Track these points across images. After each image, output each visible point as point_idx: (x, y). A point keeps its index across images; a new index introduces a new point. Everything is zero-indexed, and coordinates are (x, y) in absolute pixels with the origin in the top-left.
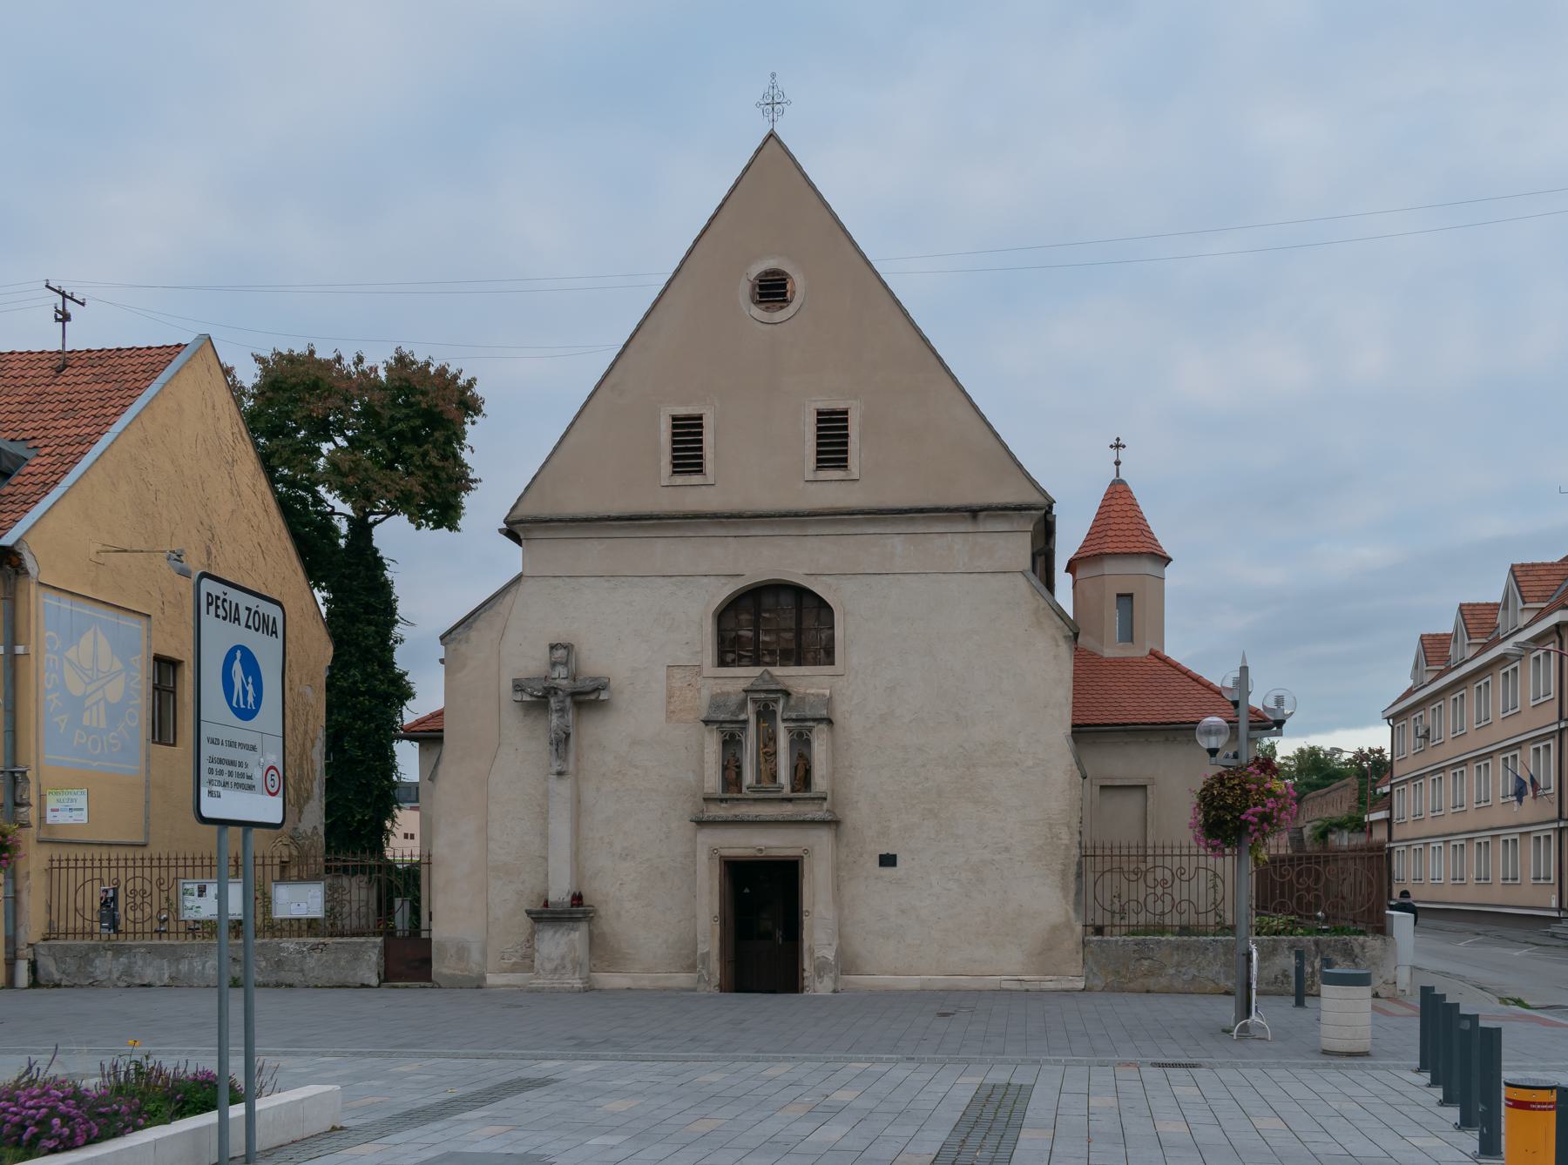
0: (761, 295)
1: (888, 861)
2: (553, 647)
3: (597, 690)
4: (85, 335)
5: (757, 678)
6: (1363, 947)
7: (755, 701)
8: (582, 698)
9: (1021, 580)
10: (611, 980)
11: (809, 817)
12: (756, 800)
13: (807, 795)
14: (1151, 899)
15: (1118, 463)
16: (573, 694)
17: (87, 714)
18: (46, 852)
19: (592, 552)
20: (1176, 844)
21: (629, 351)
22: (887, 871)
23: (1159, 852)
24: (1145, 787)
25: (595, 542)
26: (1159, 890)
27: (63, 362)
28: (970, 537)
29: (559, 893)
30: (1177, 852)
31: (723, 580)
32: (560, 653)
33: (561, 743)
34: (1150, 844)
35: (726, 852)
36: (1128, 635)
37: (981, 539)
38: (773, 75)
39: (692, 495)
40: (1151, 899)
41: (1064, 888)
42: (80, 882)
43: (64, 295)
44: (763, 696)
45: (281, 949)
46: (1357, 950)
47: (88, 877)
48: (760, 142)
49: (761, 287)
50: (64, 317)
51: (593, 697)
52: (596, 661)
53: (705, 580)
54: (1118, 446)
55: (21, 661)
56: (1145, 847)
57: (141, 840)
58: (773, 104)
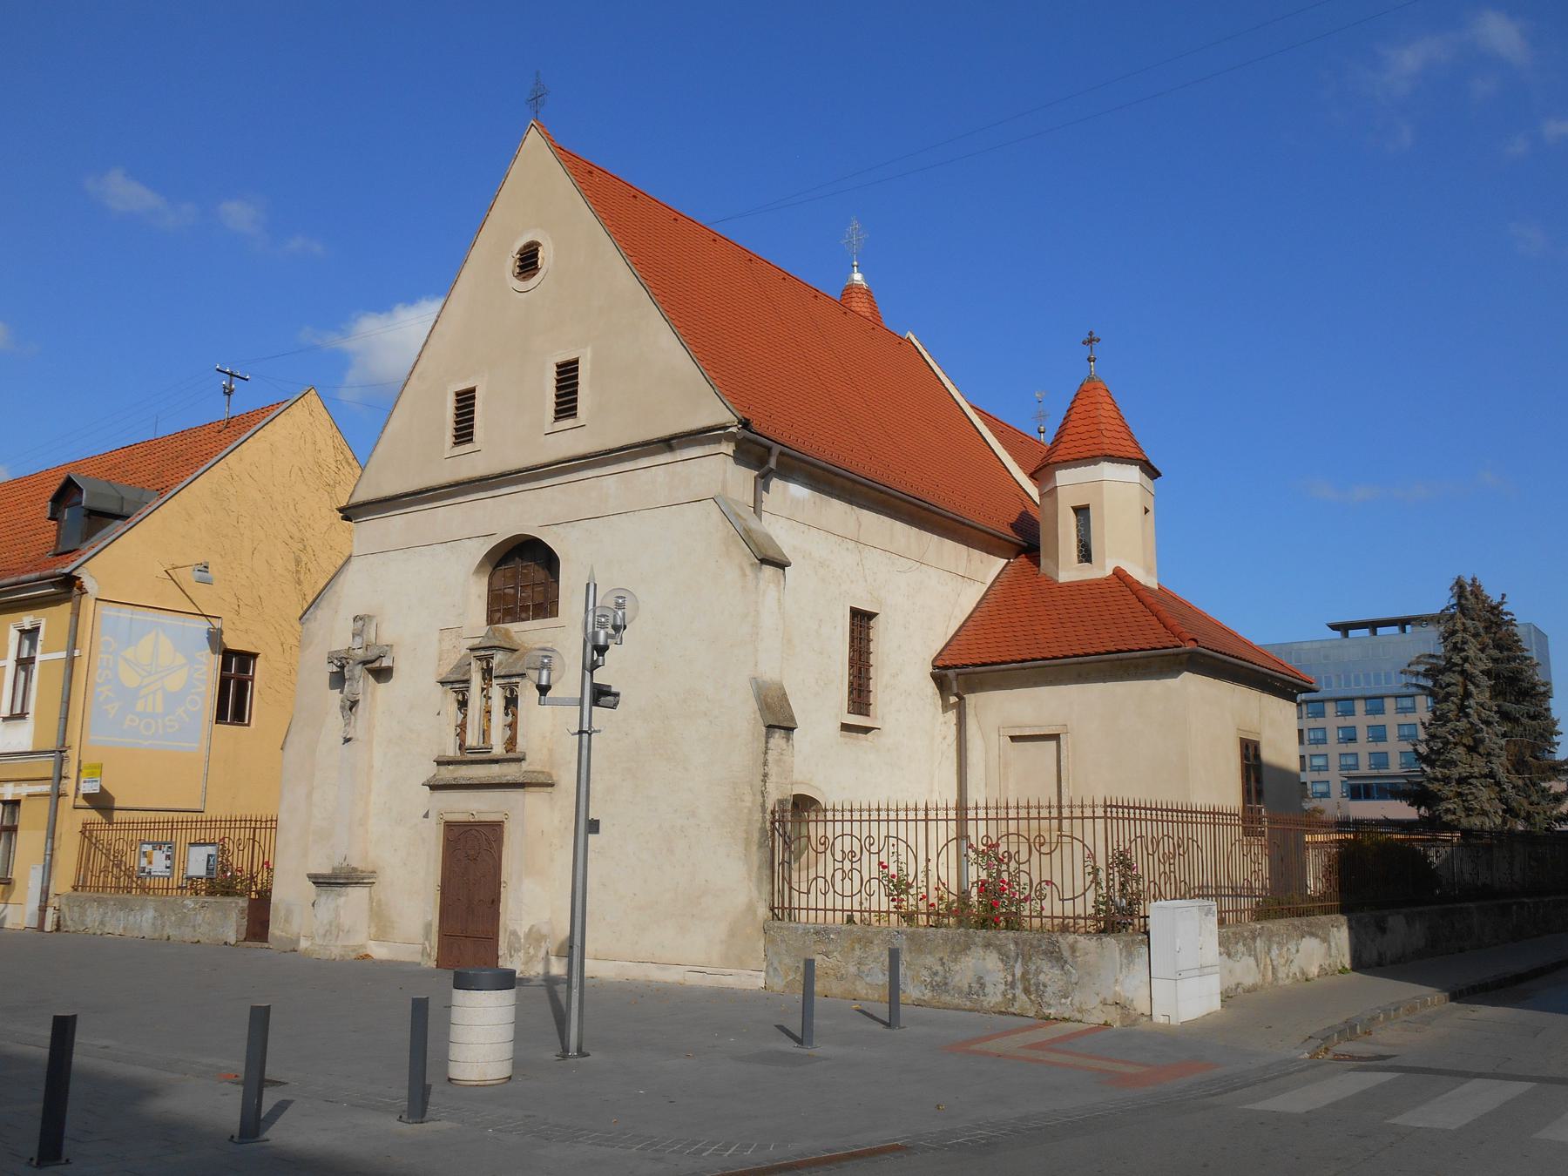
6: (1073, 949)
11: (510, 779)
14: (839, 875)
16: (365, 663)
19: (395, 524)
20: (1088, 802)
21: (431, 341)
23: (1077, 812)
34: (1065, 802)
36: (1085, 555)
38: (537, 73)
40: (839, 875)
42: (942, 842)
45: (184, 906)
46: (1066, 954)
50: (228, 392)
52: (388, 632)
54: (1091, 341)
56: (1060, 807)
57: (198, 807)
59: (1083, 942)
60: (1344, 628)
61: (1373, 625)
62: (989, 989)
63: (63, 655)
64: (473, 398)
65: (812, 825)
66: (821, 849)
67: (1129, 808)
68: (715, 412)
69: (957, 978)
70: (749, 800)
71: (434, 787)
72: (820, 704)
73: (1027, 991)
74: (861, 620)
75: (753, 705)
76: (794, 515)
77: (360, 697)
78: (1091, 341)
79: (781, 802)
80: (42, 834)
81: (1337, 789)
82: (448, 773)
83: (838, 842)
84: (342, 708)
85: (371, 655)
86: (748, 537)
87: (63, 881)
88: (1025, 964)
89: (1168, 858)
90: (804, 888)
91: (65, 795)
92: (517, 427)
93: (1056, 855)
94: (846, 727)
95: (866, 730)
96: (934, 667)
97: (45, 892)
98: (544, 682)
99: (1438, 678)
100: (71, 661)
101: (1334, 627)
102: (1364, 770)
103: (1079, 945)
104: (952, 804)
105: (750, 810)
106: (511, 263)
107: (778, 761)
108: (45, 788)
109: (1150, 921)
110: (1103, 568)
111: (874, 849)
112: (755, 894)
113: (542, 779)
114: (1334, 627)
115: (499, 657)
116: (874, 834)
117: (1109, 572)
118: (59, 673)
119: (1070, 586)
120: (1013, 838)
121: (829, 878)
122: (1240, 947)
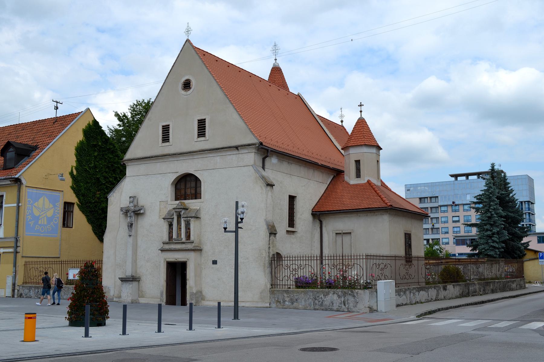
1: (215, 262)
2: (130, 197)
4: (61, 113)
5: (178, 204)
6: (357, 293)
7: (176, 212)
9: (251, 168)
10: (142, 301)
14: (291, 275)
16: (134, 212)
17: (40, 221)
18: (25, 260)
20: (361, 255)
22: (215, 265)
24: (350, 233)
26: (294, 273)
27: (56, 120)
28: (237, 155)
30: (358, 257)
31: (174, 174)
32: (132, 199)
33: (131, 225)
35: (168, 260)
36: (358, 175)
37: (240, 155)
39: (168, 149)
40: (291, 275)
43: (57, 102)
46: (355, 295)
47: (291, 263)
50: (57, 108)
53: (169, 174)
54: (361, 105)
55: (20, 208)
56: (343, 256)
57: (58, 256)
58: (188, 31)
59: (360, 291)
60: (456, 176)
61: (467, 175)
62: (334, 305)
63: (15, 205)
64: (169, 128)
66: (286, 268)
70: (265, 254)
71: (162, 250)
72: (282, 226)
73: (345, 305)
74: (292, 199)
75: (265, 227)
76: (275, 170)
78: (361, 105)
79: (273, 255)
80: (12, 265)
81: (451, 241)
82: (167, 247)
83: (291, 266)
84: (128, 226)
85: (137, 209)
86: (263, 178)
87: (20, 280)
89: (382, 269)
91: (19, 252)
92: (184, 138)
93: (304, 269)
94: (288, 231)
95: (293, 232)
97: (14, 285)
99: (483, 202)
100: (18, 207)
101: (452, 176)
102: (462, 233)
104: (318, 256)
106: (180, 85)
107: (273, 243)
108: (11, 250)
109: (377, 286)
110: (364, 180)
111: (302, 268)
112: (267, 281)
114: (452, 176)
115: (183, 212)
116: (302, 264)
117: (366, 181)
118: (14, 212)
119: (353, 185)
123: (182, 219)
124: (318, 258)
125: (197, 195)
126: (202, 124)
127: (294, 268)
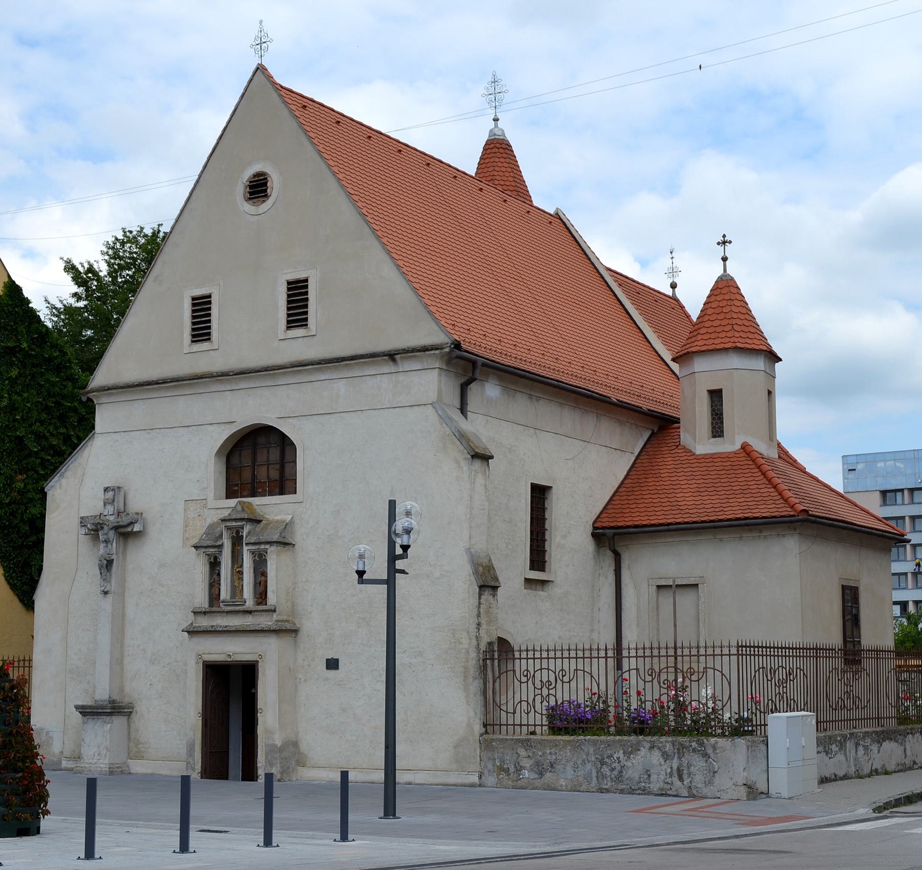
0: (251, 193)
1: (332, 664)
2: (106, 490)
3: (131, 523)
5: (234, 509)
6: (714, 748)
7: (228, 528)
8: (123, 530)
9: (430, 410)
10: (138, 767)
12: (228, 612)
13: (264, 607)
14: (538, 699)
15: (725, 259)
16: (116, 528)
20: (725, 643)
22: (332, 673)
25: (141, 402)
26: (545, 692)
28: (394, 376)
29: (102, 693)
31: (223, 427)
32: (110, 494)
33: (107, 565)
36: (717, 430)
37: (401, 377)
38: (261, 22)
40: (538, 699)
41: (466, 689)
44: (234, 524)
46: (710, 751)
47: (538, 667)
48: (251, 74)
49: (251, 187)
51: (129, 529)
52: (139, 501)
53: (211, 428)
54: (724, 243)
58: (261, 44)
59: (721, 742)
62: (654, 777)
65: (517, 662)
67: (754, 647)
68: (429, 333)
69: (630, 772)
70: (467, 643)
71: (193, 632)
72: (513, 567)
73: (681, 778)
74: (539, 493)
76: (495, 416)
77: (114, 557)
79: (490, 644)
82: (204, 622)
83: (538, 674)
84: (101, 567)
85: (124, 520)
86: (462, 437)
88: (680, 758)
89: (782, 683)
90: (511, 710)
94: (527, 581)
96: (595, 528)
98: (361, 569)
103: (719, 745)
104: (610, 646)
105: (468, 652)
107: (488, 612)
109: (769, 728)
110: (733, 443)
111: (566, 679)
112: (472, 714)
113: (289, 626)
115: (247, 528)
116: (566, 668)
117: (738, 446)
119: (705, 457)
120: (545, 672)
121: (531, 701)
122: (834, 748)
123: (245, 548)
124: (610, 653)
125: (284, 483)
126: (298, 293)
127: (545, 679)
